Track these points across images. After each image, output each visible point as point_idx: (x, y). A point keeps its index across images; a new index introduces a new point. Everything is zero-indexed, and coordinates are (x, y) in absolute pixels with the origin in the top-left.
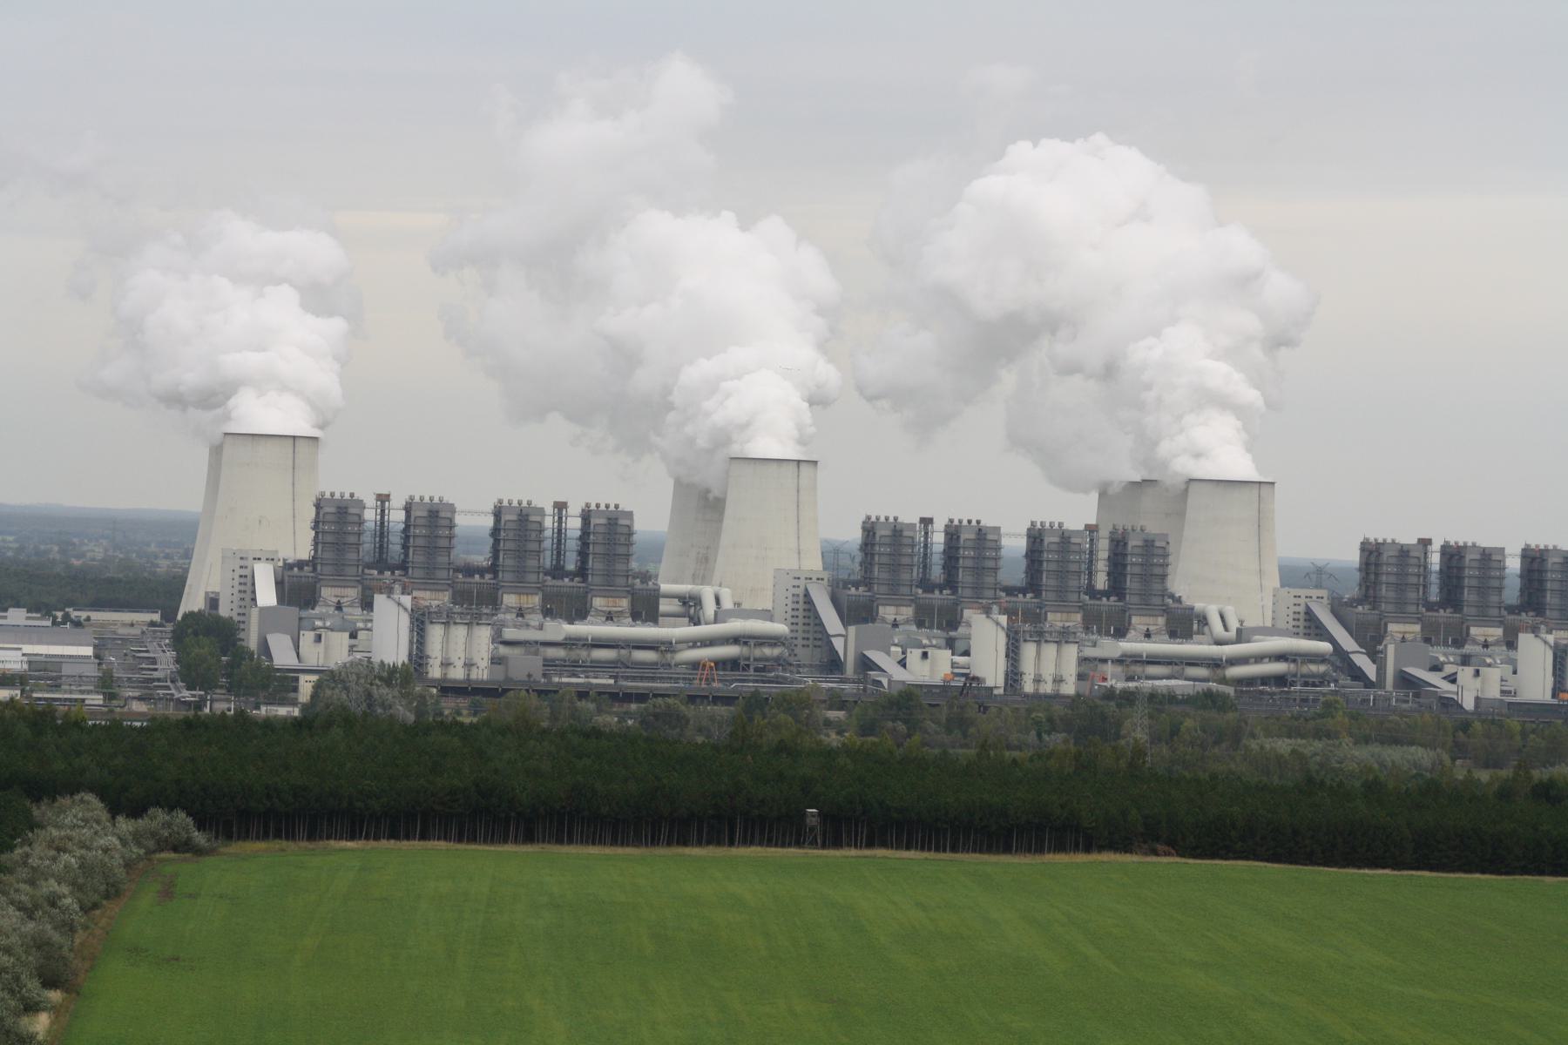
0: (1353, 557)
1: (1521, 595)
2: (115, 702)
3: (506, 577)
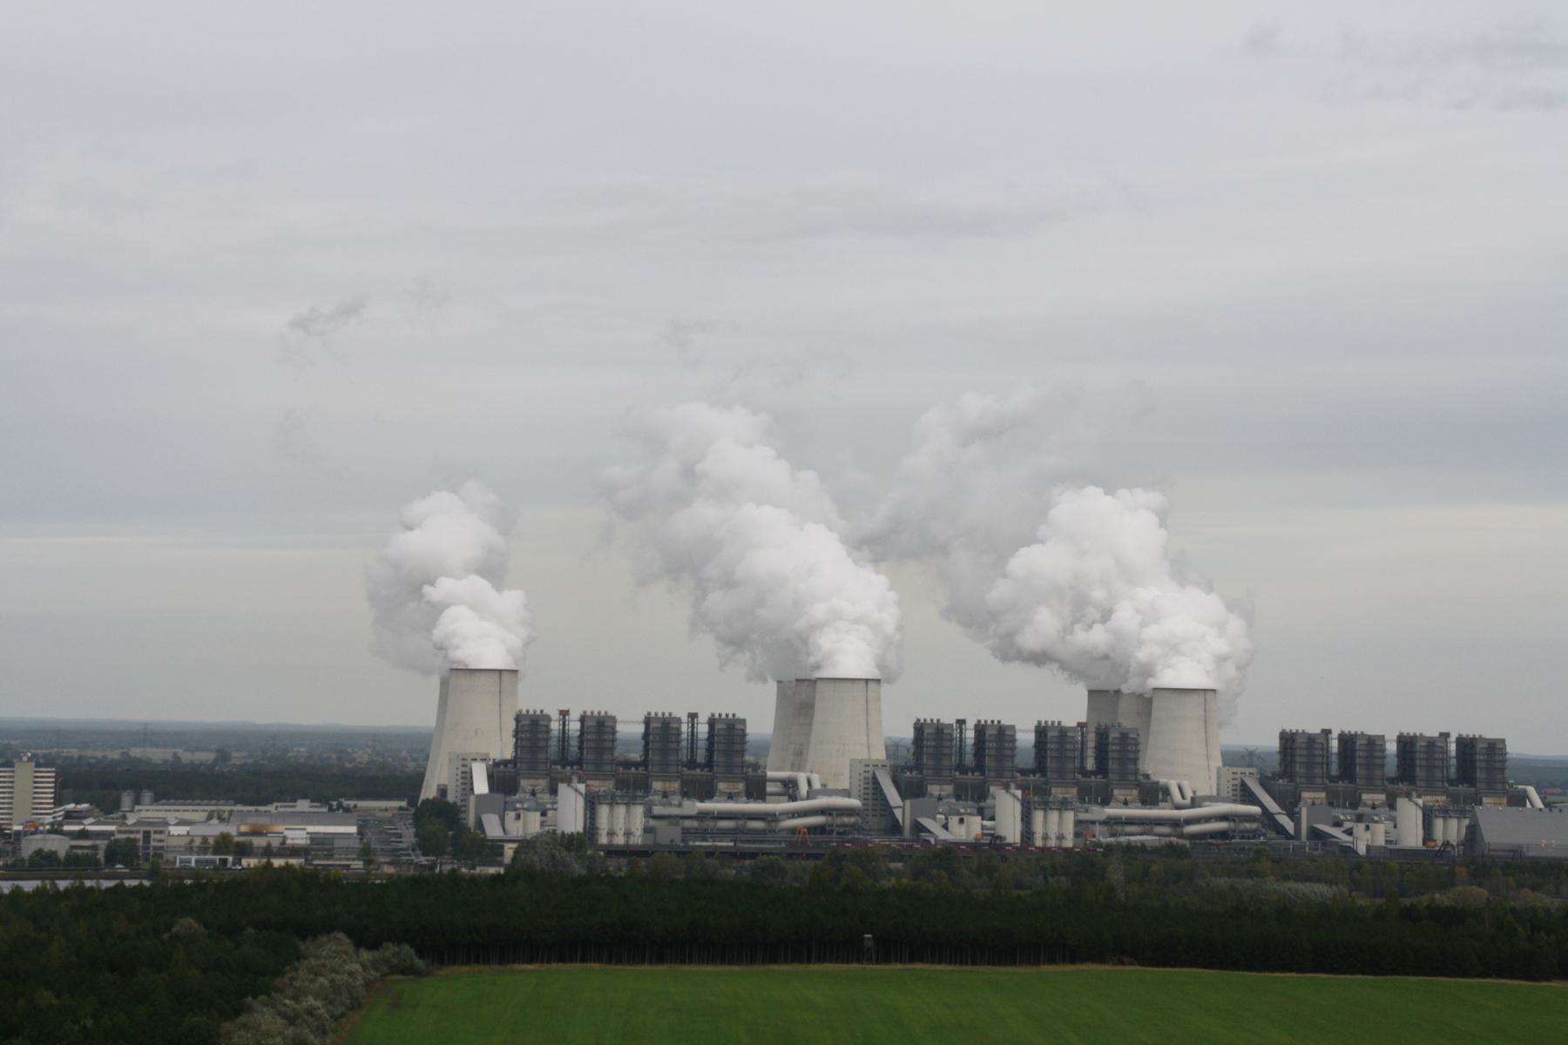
0: (1274, 744)
1: (1398, 770)
2: (372, 866)
3: (654, 769)
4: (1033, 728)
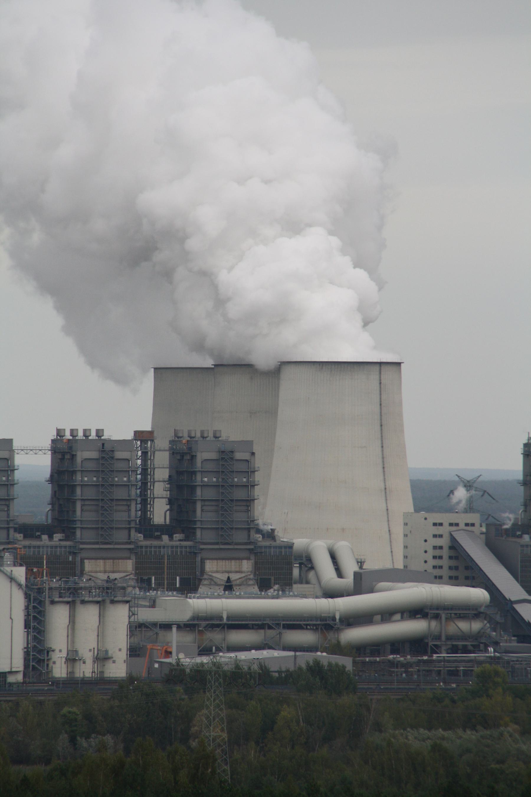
4: (48, 444)
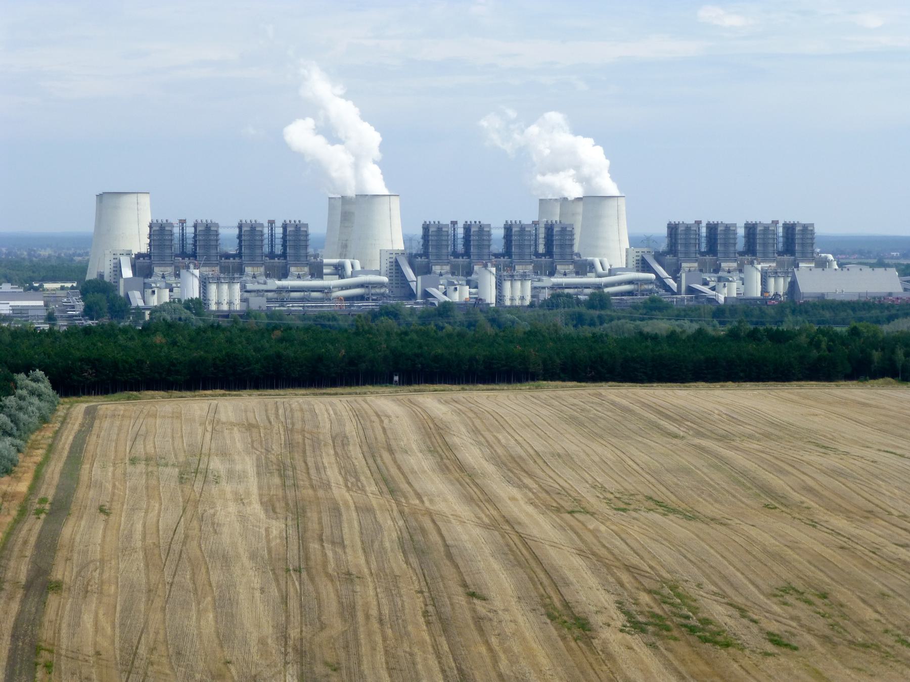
4: (503, 226)
